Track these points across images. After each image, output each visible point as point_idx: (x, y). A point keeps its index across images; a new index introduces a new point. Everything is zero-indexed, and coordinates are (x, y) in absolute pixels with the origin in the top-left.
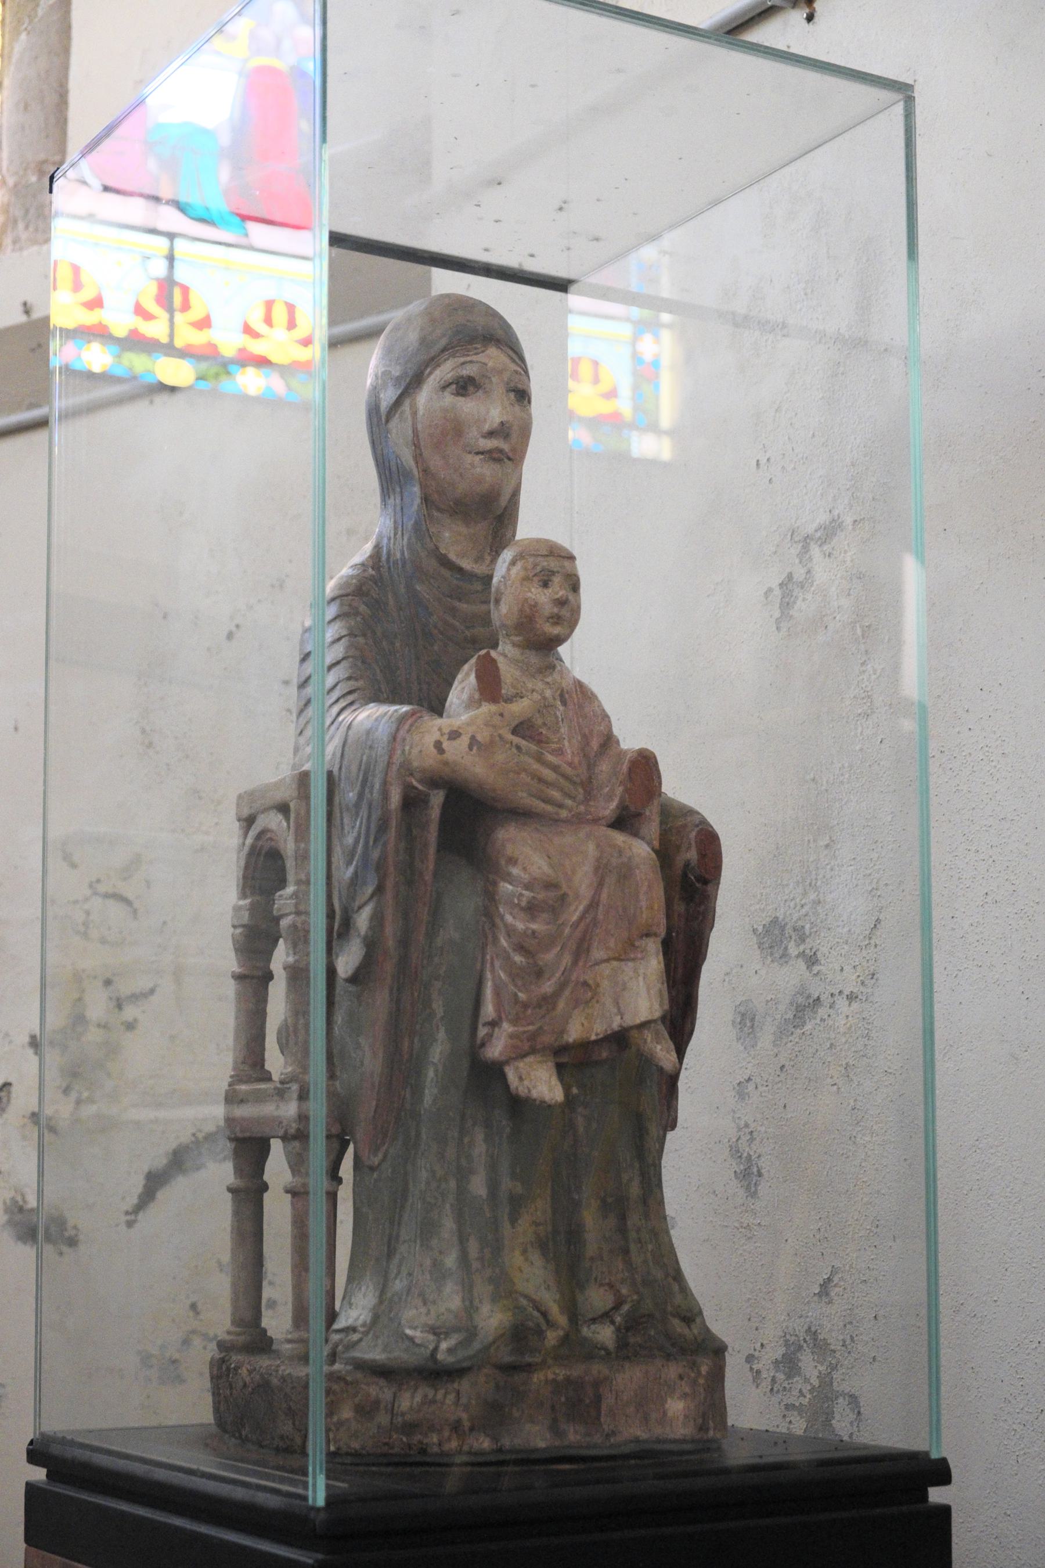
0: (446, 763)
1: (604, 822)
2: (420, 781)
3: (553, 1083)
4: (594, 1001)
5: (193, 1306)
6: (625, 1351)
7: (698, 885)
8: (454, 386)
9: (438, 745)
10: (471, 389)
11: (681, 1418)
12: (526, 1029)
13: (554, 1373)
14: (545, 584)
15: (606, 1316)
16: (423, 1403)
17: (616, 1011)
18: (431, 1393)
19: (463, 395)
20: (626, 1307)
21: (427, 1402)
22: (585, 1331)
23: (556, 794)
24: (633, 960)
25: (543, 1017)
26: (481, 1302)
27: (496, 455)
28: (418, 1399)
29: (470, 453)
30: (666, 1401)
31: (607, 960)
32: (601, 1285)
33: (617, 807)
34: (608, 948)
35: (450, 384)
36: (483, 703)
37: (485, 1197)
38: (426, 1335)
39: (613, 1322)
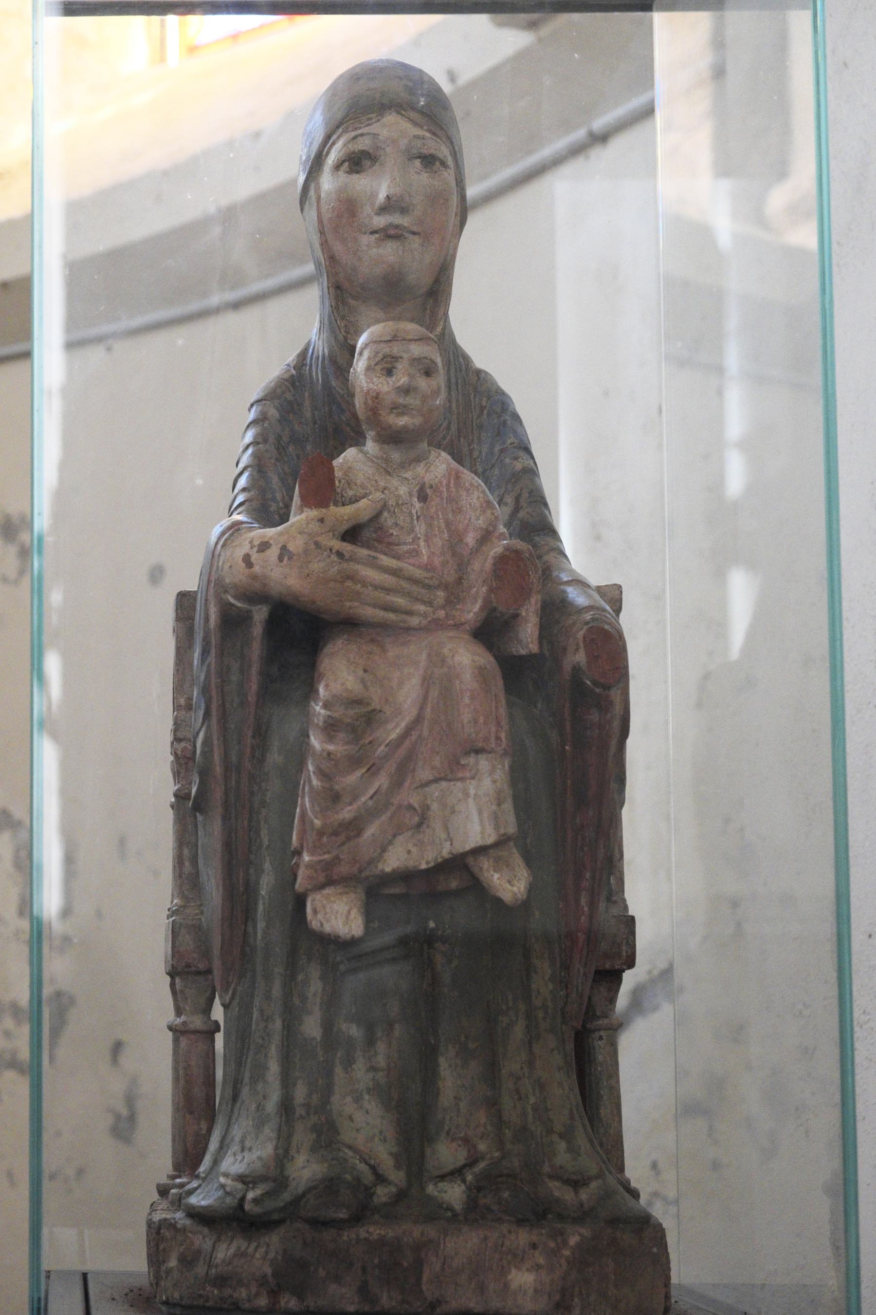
0: (255, 577)
1: (467, 627)
2: (235, 597)
3: (353, 915)
4: (425, 826)
5: (654, 1166)
6: (474, 1213)
7: (597, 690)
8: (347, 164)
9: (247, 559)
10: (367, 163)
11: (531, 1292)
12: (322, 858)
13: (368, 1232)
14: (389, 372)
15: (457, 1173)
16: (235, 1255)
17: (446, 836)
18: (244, 1245)
19: (357, 172)
20: (482, 1165)
21: (242, 1255)
22: (430, 1189)
23: (400, 601)
24: (462, 779)
25: (343, 844)
26: (298, 1152)
27: (392, 232)
28: (232, 1251)
29: (365, 233)
30: (510, 1272)
31: (436, 780)
32: (453, 1140)
33: (482, 609)
34: (433, 768)
35: (344, 161)
36: (305, 509)
37: (319, 1039)
38: (236, 1183)
39: (464, 1181)
